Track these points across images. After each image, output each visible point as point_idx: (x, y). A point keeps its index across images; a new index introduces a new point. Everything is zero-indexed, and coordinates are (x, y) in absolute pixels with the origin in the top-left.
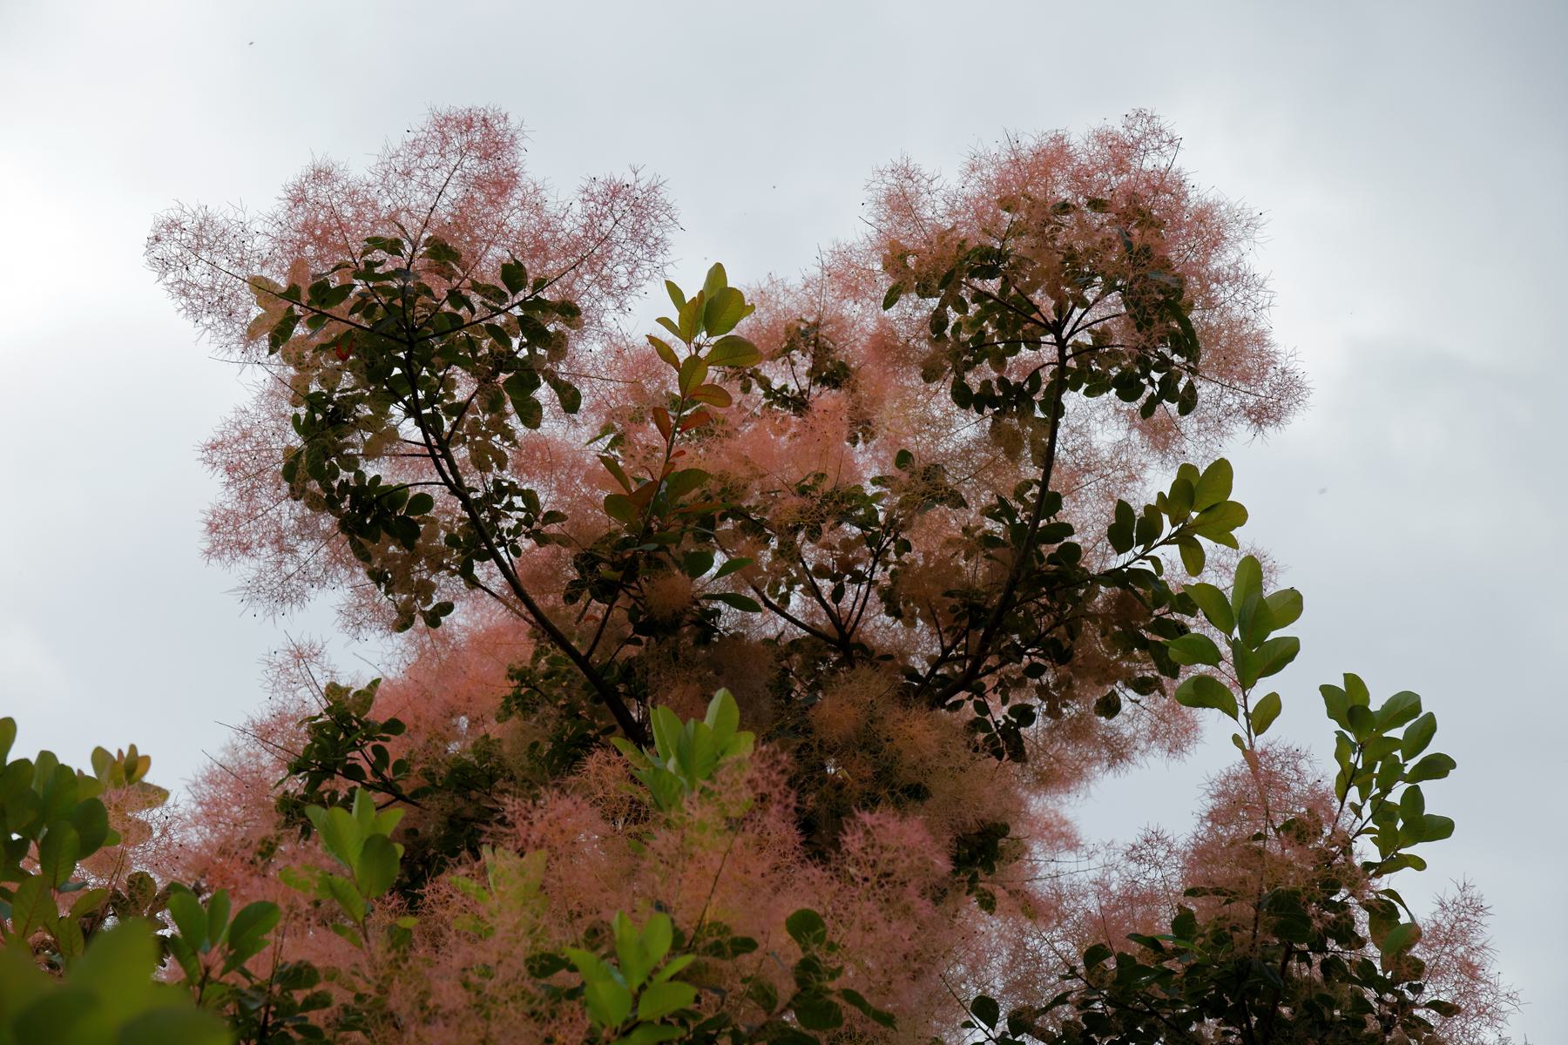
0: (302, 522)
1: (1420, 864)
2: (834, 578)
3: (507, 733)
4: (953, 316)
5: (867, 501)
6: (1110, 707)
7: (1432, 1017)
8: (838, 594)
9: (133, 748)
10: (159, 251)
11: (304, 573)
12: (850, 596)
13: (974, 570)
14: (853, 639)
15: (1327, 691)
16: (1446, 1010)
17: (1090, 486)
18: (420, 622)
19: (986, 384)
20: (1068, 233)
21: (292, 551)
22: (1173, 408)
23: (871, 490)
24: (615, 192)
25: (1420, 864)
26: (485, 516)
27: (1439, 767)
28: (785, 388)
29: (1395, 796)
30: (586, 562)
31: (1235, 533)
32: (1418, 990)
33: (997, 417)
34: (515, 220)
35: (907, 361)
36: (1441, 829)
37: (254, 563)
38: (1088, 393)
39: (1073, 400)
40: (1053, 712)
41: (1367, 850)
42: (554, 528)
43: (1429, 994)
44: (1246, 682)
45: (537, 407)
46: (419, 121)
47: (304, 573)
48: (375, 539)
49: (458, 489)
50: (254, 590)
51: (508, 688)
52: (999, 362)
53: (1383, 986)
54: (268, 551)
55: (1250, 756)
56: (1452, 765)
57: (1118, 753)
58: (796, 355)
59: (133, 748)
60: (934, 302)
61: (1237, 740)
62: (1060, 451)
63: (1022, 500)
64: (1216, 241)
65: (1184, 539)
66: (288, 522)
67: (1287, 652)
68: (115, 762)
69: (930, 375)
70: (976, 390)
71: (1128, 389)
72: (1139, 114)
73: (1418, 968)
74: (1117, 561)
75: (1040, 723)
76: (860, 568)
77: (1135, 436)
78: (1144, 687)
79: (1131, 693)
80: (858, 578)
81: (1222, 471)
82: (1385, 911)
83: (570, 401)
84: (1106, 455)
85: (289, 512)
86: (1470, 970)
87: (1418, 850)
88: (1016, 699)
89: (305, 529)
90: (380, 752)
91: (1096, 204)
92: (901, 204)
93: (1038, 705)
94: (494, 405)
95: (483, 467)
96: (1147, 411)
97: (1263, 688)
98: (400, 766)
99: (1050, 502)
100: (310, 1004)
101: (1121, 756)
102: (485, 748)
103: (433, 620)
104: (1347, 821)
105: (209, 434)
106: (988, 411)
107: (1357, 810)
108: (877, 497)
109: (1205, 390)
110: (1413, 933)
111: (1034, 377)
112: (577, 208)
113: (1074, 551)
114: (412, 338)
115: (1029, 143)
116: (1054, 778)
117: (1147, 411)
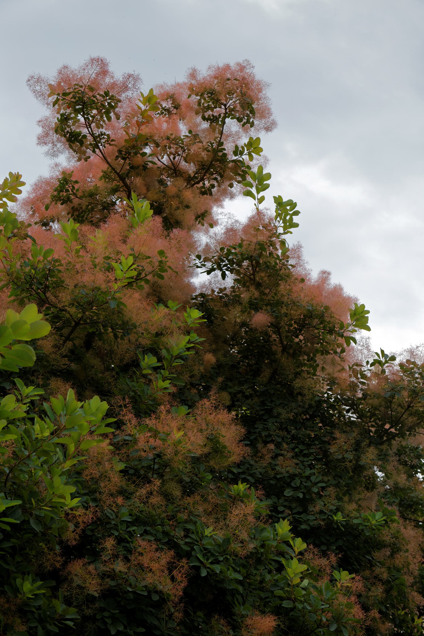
1: (291, 233)
2: (174, 155)
4: (203, 101)
6: (231, 186)
7: (290, 267)
8: (174, 158)
9: (18, 173)
10: (29, 83)
12: (177, 158)
15: (274, 197)
16: (293, 266)
18: (83, 160)
19: (209, 116)
20: (229, 85)
21: (56, 145)
23: (182, 137)
24: (130, 76)
25: (291, 233)
27: (297, 213)
28: (165, 107)
30: (120, 151)
32: (288, 261)
34: (108, 80)
36: (296, 225)
37: (47, 147)
38: (231, 119)
39: (227, 120)
40: (219, 186)
41: (281, 230)
42: (113, 143)
45: (111, 117)
46: (87, 58)
47: (59, 151)
48: (74, 143)
50: (47, 154)
53: (280, 260)
54: (50, 145)
55: (257, 209)
56: (300, 213)
57: (232, 196)
58: (169, 100)
59: (18, 173)
60: (198, 98)
61: (255, 204)
63: (215, 141)
64: (260, 91)
65: (250, 154)
66: (55, 139)
67: (267, 187)
69: (197, 113)
71: (239, 120)
72: (246, 60)
73: (288, 257)
74: (235, 158)
75: (215, 189)
77: (241, 130)
78: (239, 182)
80: (179, 155)
81: (258, 139)
82: (283, 243)
84: (234, 133)
85: (55, 137)
87: (291, 230)
89: (58, 140)
90: (73, 187)
91: (236, 79)
92: (193, 75)
95: (98, 128)
97: (262, 194)
98: (77, 190)
99: (221, 144)
101: (233, 197)
102: (96, 186)
103: (86, 160)
104: (277, 224)
105: (38, 119)
106: (209, 122)
108: (184, 139)
109: (256, 122)
110: (288, 250)
112: (121, 79)
114: (84, 104)
115: (221, 65)
116: (218, 201)
117: (243, 125)
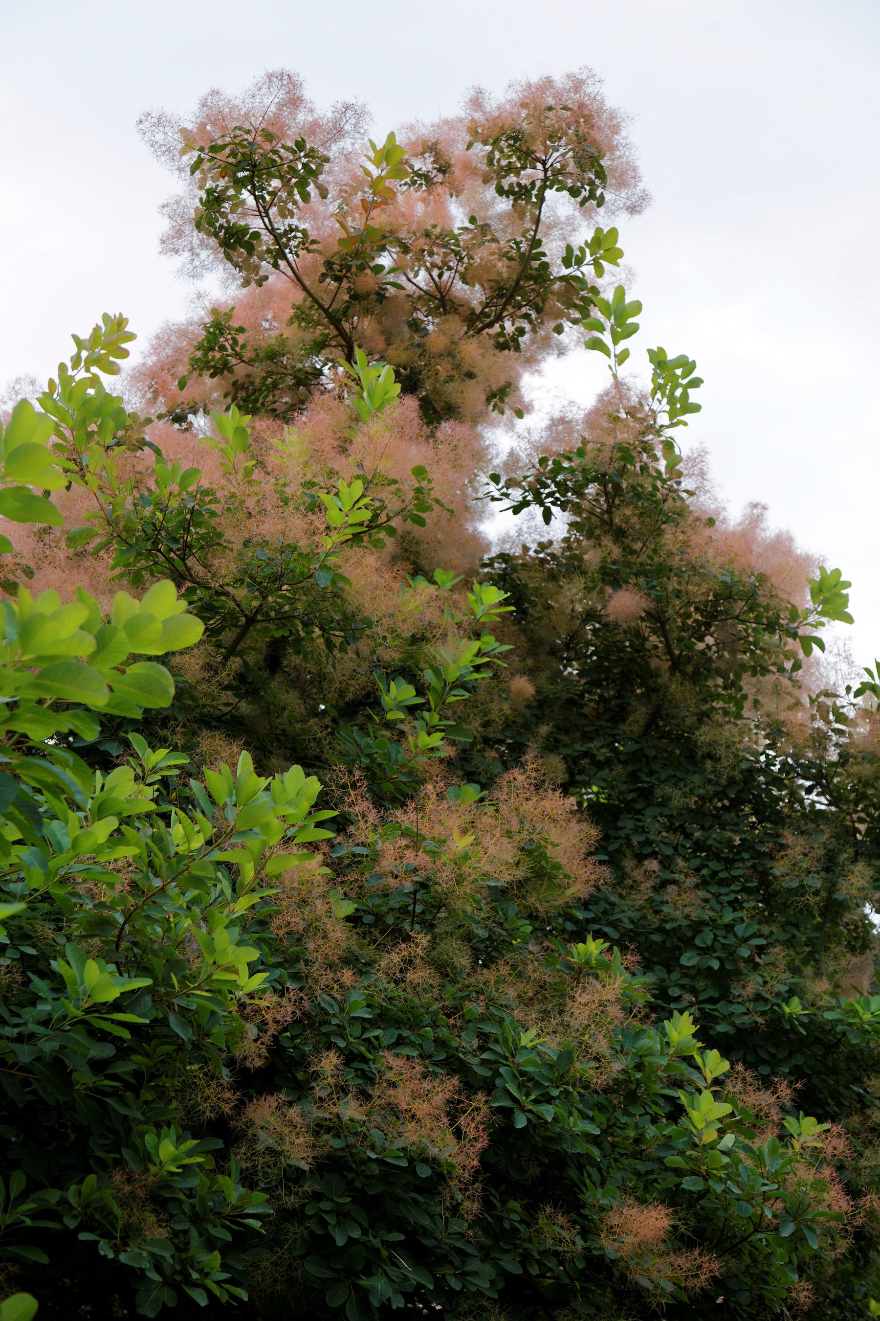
0: (202, 241)
1: (685, 424)
2: (440, 268)
3: (291, 333)
4: (497, 155)
5: (455, 237)
6: (559, 330)
7: (684, 495)
8: (440, 276)
9: (121, 314)
10: (141, 126)
11: (204, 267)
13: (502, 266)
14: (447, 298)
15: (650, 351)
17: (556, 233)
18: (253, 284)
19: (511, 185)
20: (551, 119)
21: (198, 255)
22: (594, 203)
23: (456, 232)
25: (685, 424)
26: (284, 240)
27: (696, 383)
29: (678, 392)
30: (329, 264)
31: (619, 261)
32: (679, 483)
33: (515, 200)
35: (476, 174)
36: (696, 408)
39: (549, 194)
40: (534, 330)
41: (663, 419)
42: (315, 246)
43: (684, 486)
44: (615, 342)
45: (309, 194)
46: (260, 74)
49: (272, 231)
51: (292, 312)
52: (518, 174)
56: (702, 382)
57: (562, 351)
58: (427, 155)
59: (121, 314)
60: (489, 148)
61: (610, 367)
62: (543, 217)
64: (616, 130)
65: (596, 264)
67: (634, 329)
68: (113, 321)
70: (506, 188)
71: (574, 192)
73: (680, 474)
74: (565, 272)
76: (451, 264)
77: (577, 213)
78: (575, 322)
79: (571, 325)
80: (450, 268)
81: (614, 232)
83: (324, 193)
84: (563, 219)
86: (702, 474)
87: (686, 418)
88: (518, 324)
89: (202, 244)
90: (235, 340)
91: (565, 108)
92: (476, 102)
93: (527, 327)
94: (290, 194)
95: (284, 216)
96: (582, 204)
97: (623, 344)
98: (243, 347)
99: (536, 243)
100: (210, 502)
103: (260, 283)
104: (656, 406)
107: (660, 402)
108: (460, 234)
109: (608, 197)
110: (679, 459)
111: (533, 183)
113: (545, 266)
115: (534, 79)
117: (582, 204)
